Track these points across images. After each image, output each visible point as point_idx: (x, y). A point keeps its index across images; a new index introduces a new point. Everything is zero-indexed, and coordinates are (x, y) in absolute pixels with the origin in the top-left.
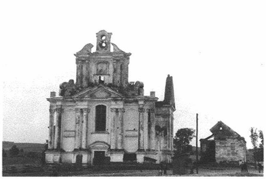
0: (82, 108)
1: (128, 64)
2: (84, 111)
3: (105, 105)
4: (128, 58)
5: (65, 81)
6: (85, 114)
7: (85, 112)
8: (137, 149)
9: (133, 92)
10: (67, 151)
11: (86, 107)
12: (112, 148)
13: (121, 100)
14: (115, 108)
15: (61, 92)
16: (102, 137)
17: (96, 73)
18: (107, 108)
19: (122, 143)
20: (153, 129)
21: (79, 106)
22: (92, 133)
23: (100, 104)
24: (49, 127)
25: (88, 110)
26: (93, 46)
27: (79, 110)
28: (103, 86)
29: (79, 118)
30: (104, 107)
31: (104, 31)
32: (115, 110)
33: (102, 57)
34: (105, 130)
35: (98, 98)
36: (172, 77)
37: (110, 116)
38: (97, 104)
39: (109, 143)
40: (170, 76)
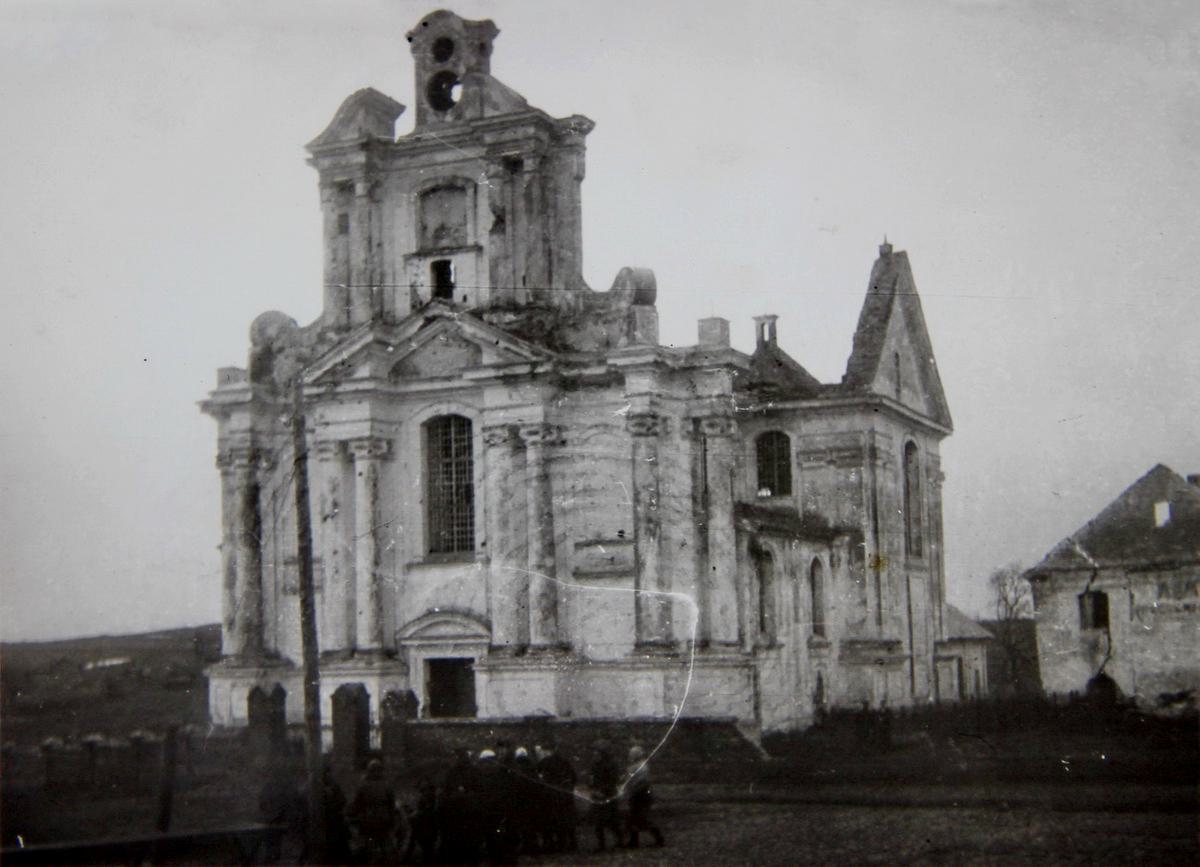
0: (344, 437)
1: (579, 178)
2: (358, 454)
3: (467, 413)
4: (578, 149)
5: (296, 319)
6: (361, 466)
7: (362, 458)
8: (632, 637)
9: (603, 331)
10: (594, 652)
11: (364, 430)
12: (500, 636)
13: (533, 377)
14: (503, 426)
15: (758, 446)
16: (437, 585)
17: (414, 250)
18: (476, 429)
19: (552, 606)
20: (721, 523)
21: (331, 428)
22: (410, 567)
23: (444, 410)
24: (220, 547)
25: (383, 451)
26: (401, 108)
27: (332, 446)
28: (448, 313)
29: (334, 490)
30: (464, 424)
31: (441, 15)
32: (506, 434)
33: (440, 157)
34: (472, 547)
35: (432, 379)
36: (902, 255)
37: (490, 467)
38: (427, 413)
39: (479, 607)
40: (896, 250)
